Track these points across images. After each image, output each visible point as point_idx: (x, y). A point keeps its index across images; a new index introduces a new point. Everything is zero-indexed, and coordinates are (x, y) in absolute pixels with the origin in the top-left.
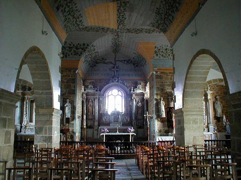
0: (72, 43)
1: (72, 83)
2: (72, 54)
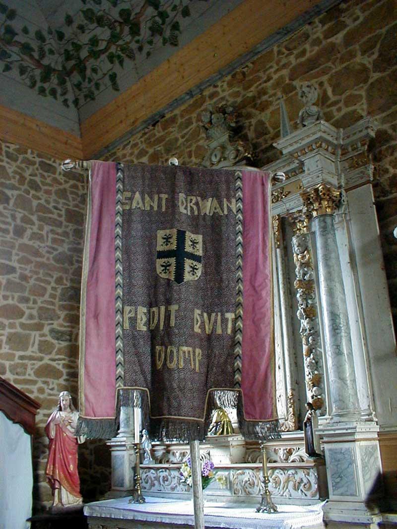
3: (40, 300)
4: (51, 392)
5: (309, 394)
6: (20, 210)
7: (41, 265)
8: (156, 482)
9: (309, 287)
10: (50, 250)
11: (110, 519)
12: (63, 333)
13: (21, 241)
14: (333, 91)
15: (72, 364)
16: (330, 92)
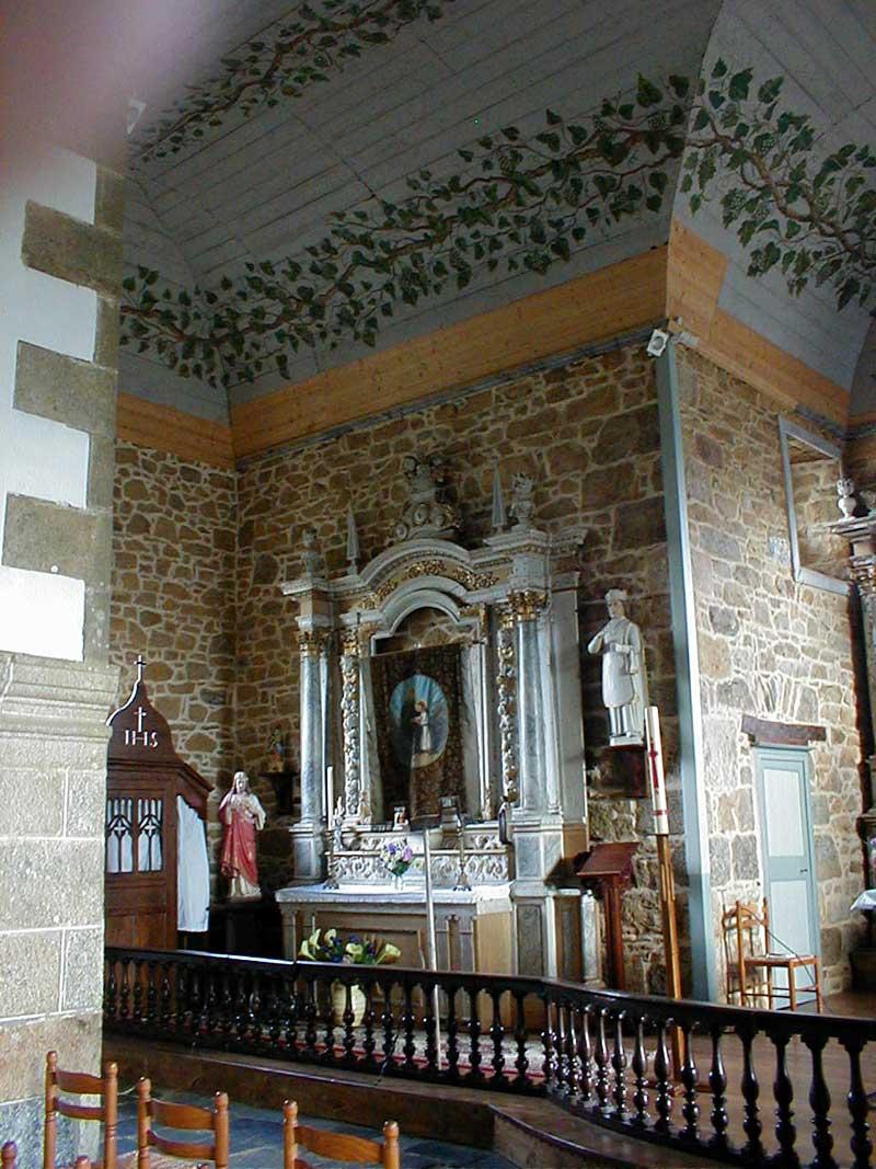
0: (553, 119)
1: (640, 449)
2: (592, 213)
3: (189, 654)
4: (205, 768)
5: (506, 787)
6: (162, 539)
7: (188, 609)
8: (348, 870)
9: (511, 683)
10: (199, 588)
11: (308, 903)
12: (215, 694)
13: (165, 580)
14: (552, 467)
15: (226, 732)
16: (548, 468)
